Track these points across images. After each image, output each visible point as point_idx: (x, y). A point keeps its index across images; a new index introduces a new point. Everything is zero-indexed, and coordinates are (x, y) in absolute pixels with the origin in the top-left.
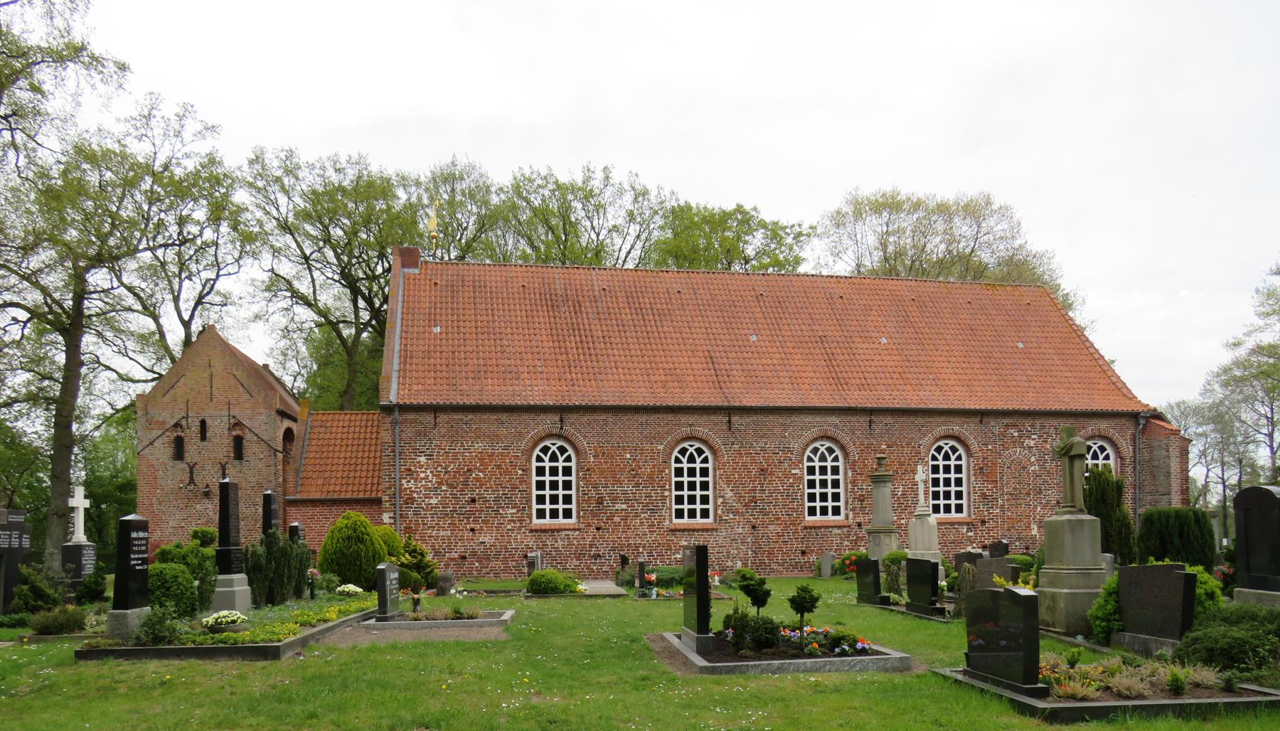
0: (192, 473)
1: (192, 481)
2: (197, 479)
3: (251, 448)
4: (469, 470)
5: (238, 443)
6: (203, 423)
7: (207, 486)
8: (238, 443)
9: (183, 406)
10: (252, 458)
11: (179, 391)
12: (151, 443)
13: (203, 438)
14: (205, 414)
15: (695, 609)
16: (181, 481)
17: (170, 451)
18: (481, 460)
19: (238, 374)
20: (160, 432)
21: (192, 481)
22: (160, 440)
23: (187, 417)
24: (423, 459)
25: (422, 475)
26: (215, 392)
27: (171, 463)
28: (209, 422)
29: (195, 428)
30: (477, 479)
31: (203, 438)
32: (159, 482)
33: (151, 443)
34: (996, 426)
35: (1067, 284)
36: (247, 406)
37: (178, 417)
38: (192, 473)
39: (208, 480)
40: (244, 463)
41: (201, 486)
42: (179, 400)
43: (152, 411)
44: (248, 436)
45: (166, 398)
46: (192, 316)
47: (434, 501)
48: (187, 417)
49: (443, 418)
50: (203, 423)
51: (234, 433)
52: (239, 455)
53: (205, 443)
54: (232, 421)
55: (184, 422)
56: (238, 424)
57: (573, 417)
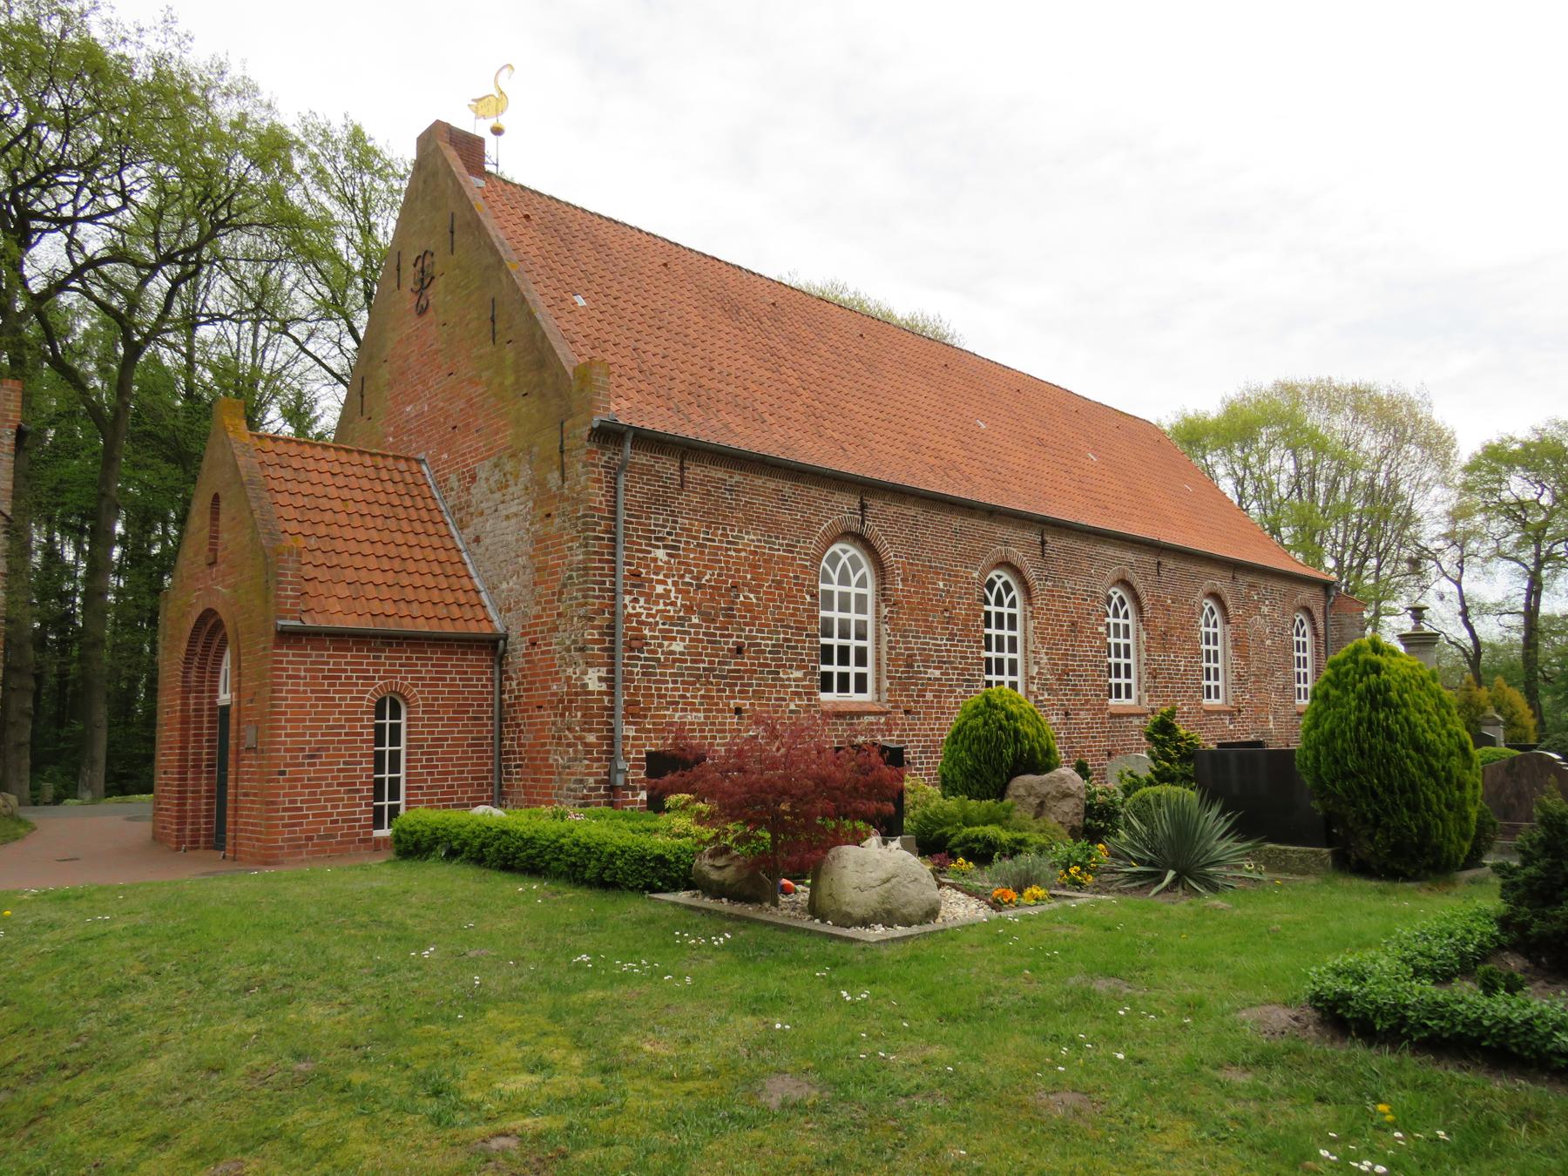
4: (734, 586)
18: (754, 567)
24: (661, 554)
25: (660, 589)
30: (748, 607)
34: (1244, 580)
47: (678, 647)
49: (695, 471)
57: (875, 505)
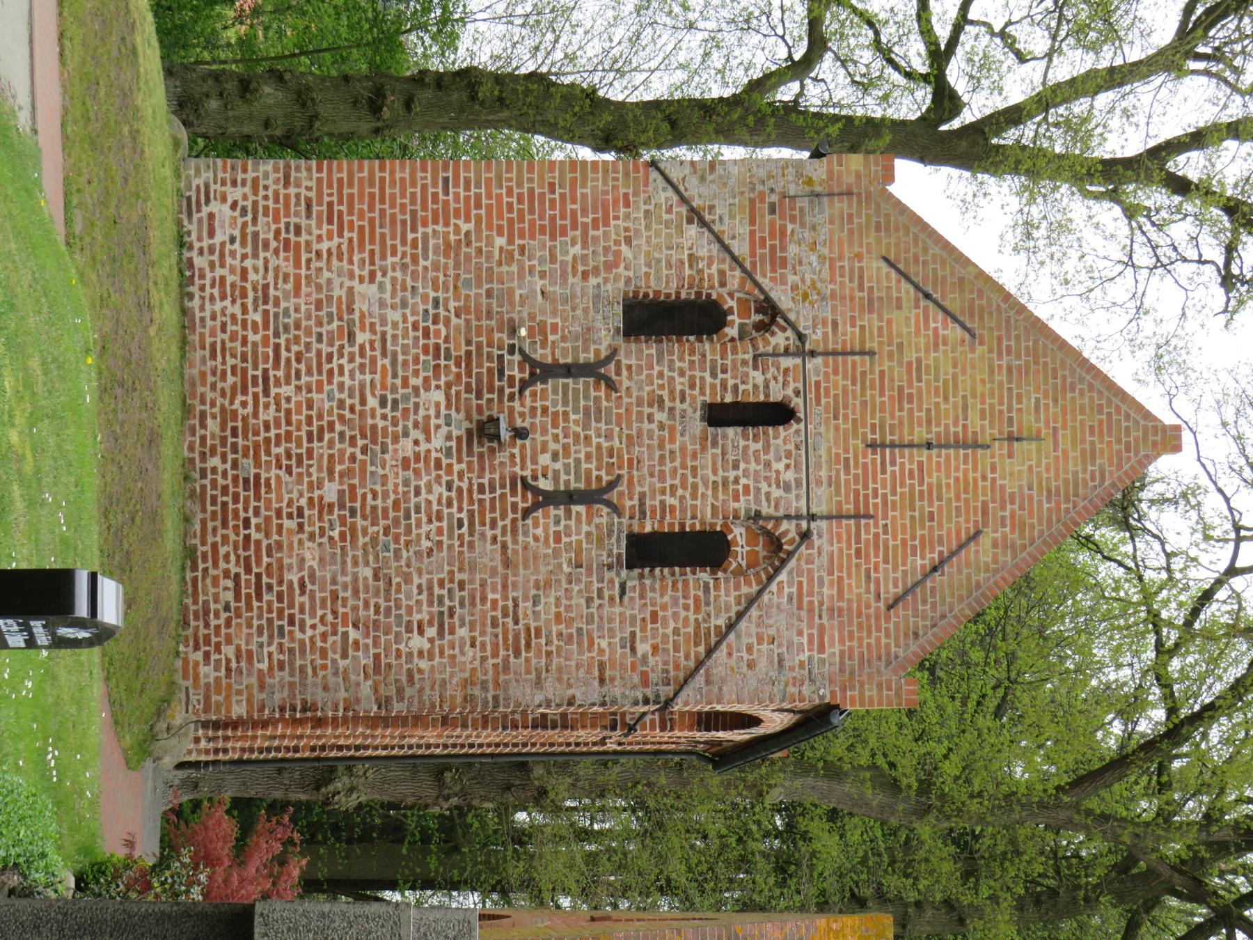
0: (569, 371)
1: (541, 372)
2: (551, 392)
3: (679, 599)
5: (702, 549)
6: (779, 414)
7: (520, 434)
8: (702, 549)
9: (849, 335)
10: (633, 608)
11: (907, 320)
12: (696, 216)
13: (718, 415)
14: (820, 429)
15: (24, 566)
16: (539, 330)
17: (665, 283)
19: (983, 551)
20: (740, 248)
21: (541, 372)
22: (706, 249)
23: (802, 350)
26: (907, 461)
27: (614, 289)
28: (782, 437)
29: (756, 384)
31: (718, 415)
32: (538, 246)
33: (696, 216)
35: (930, 169)
36: (855, 588)
37: (802, 316)
38: (569, 371)
39: (546, 436)
40: (616, 577)
41: (521, 410)
42: (872, 321)
43: (823, 215)
44: (726, 593)
45: (875, 268)
46: (1181, 186)
48: (802, 350)
50: (779, 414)
51: (738, 533)
52: (648, 551)
53: (697, 425)
54: (789, 529)
55: (780, 339)
56: (776, 552)
